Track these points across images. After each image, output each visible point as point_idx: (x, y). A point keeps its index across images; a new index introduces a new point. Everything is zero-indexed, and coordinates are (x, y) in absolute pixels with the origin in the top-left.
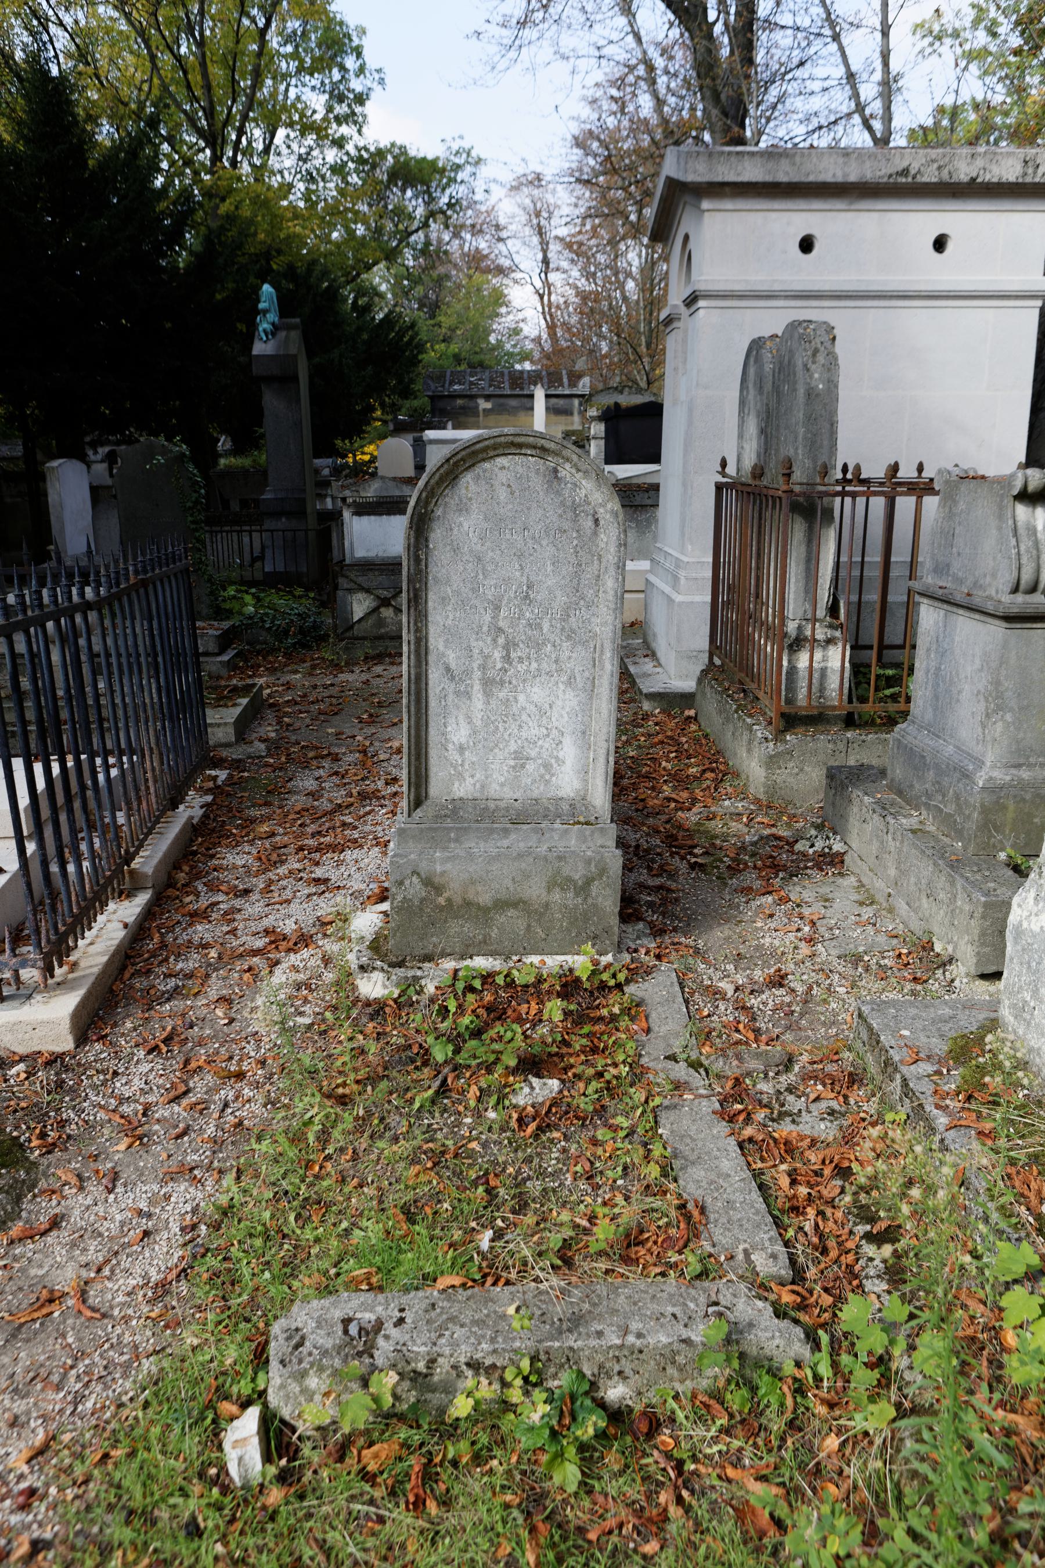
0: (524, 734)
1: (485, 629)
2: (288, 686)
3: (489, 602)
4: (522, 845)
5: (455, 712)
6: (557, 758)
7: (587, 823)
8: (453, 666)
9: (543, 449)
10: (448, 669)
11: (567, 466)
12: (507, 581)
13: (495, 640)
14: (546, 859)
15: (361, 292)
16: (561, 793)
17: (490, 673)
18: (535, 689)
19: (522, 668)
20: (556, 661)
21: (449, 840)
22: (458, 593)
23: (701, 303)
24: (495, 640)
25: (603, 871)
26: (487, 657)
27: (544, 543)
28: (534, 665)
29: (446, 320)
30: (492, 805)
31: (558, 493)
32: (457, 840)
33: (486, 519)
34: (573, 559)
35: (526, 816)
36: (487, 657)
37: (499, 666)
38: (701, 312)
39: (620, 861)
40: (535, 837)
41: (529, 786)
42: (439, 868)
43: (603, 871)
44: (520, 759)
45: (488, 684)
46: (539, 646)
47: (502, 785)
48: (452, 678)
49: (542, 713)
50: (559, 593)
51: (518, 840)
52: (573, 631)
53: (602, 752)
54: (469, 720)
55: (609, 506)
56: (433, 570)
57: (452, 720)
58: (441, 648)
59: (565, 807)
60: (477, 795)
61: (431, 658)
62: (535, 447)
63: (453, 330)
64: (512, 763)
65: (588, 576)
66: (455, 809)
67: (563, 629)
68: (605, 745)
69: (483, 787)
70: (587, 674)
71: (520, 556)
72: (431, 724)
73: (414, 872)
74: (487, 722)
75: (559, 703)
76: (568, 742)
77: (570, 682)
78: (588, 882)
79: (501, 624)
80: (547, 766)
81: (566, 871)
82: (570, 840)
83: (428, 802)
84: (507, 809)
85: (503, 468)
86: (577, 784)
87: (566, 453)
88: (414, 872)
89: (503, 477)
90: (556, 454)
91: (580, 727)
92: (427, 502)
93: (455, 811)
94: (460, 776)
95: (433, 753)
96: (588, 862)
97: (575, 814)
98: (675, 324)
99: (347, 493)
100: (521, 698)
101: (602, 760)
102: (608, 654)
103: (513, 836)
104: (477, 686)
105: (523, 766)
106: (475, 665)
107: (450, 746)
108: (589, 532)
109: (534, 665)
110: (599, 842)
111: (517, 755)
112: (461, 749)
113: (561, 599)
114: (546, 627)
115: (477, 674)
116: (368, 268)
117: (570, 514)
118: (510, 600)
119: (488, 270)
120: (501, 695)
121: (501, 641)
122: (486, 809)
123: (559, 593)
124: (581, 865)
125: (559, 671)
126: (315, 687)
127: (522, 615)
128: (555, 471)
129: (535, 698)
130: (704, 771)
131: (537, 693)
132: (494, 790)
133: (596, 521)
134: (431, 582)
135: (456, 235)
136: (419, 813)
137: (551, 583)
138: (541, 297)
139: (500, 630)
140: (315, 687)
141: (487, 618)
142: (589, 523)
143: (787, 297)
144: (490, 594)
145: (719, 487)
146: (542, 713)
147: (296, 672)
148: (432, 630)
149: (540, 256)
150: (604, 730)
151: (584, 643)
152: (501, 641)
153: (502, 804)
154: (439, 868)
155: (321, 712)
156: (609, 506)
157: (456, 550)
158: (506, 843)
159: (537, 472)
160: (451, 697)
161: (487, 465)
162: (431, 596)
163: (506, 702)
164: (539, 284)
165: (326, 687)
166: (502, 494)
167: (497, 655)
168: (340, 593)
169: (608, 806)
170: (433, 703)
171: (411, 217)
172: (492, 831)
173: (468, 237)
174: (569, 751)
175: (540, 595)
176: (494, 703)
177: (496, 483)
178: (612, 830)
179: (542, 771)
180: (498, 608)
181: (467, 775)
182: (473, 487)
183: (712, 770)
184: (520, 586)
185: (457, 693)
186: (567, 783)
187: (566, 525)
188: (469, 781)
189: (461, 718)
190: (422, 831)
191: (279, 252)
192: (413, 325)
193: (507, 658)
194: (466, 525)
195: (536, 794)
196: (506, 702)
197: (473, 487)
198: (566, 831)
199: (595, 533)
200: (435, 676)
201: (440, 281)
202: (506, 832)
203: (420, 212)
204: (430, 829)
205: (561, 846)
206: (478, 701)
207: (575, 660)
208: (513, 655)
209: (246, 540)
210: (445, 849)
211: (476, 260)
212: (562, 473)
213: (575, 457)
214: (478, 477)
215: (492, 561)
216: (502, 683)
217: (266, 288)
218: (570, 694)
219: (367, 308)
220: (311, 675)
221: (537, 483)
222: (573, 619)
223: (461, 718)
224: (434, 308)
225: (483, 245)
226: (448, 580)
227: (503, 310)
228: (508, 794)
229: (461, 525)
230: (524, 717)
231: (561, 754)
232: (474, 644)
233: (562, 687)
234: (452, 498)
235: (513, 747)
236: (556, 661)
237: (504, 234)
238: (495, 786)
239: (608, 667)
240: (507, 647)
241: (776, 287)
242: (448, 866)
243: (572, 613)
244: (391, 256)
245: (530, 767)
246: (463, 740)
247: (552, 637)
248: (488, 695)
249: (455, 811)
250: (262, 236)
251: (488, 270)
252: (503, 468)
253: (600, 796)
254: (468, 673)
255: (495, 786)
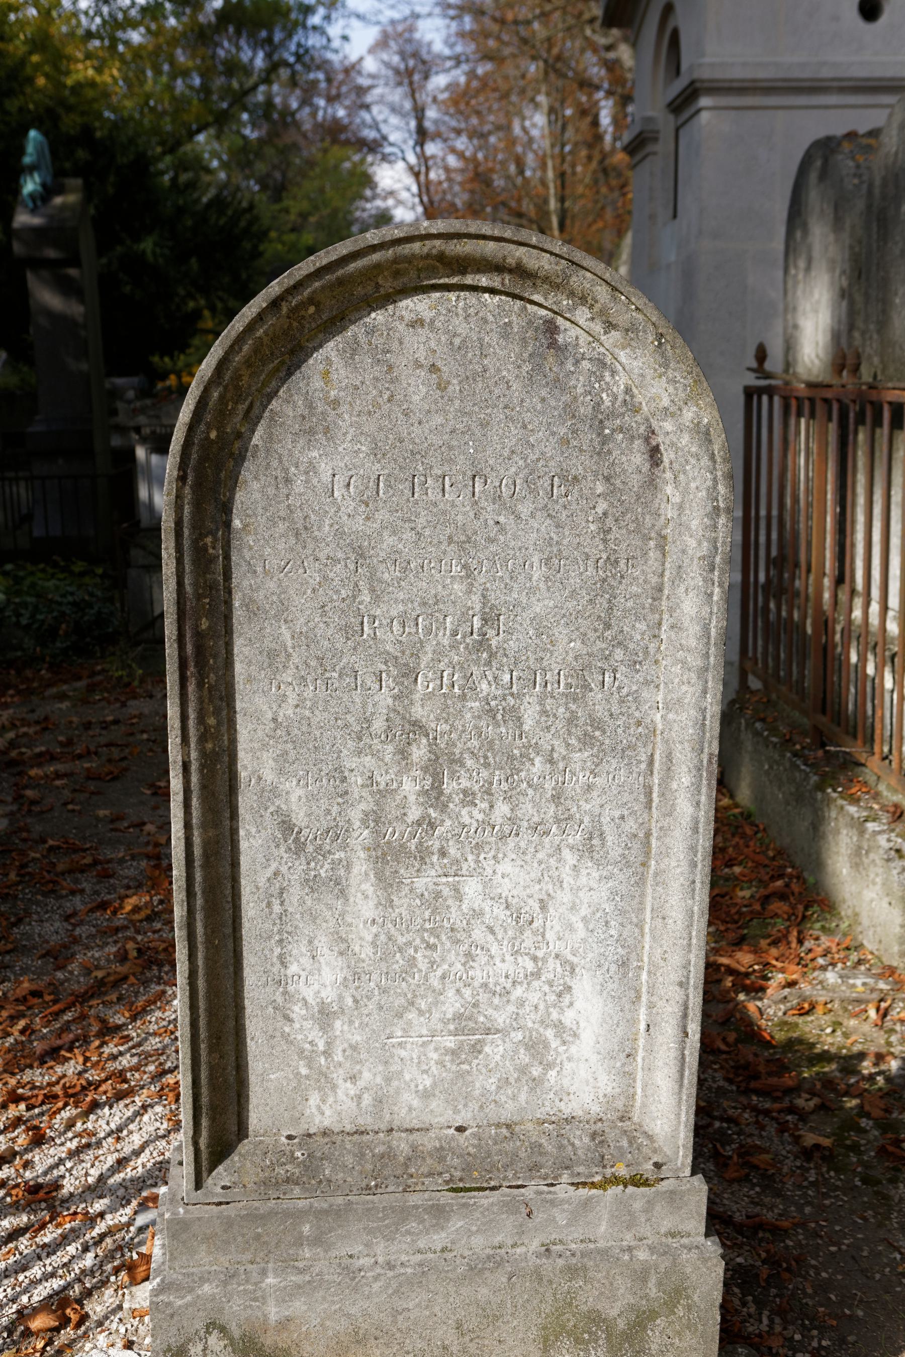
0: (478, 975)
1: (379, 725)
2: (45, 725)
3: (388, 659)
4: (478, 1241)
5: (307, 930)
6: (559, 1027)
7: (638, 1181)
8: (299, 818)
9: (520, 272)
10: (287, 826)
11: (582, 315)
12: (432, 606)
13: (403, 753)
14: (538, 1275)
15: (182, 166)
16: (569, 1108)
17: (395, 833)
18: (505, 867)
19: (471, 816)
20: (556, 798)
21: (299, 1242)
22: (307, 638)
23: (704, 101)
24: (403, 753)
25: (676, 1294)
26: (385, 793)
27: (524, 509)
28: (502, 809)
29: (295, 205)
30: (402, 1145)
31: (558, 384)
32: (317, 1241)
33: (376, 452)
34: (596, 549)
35: (484, 1169)
36: (385, 793)
37: (414, 814)
38: (705, 116)
39: (718, 1270)
40: (509, 1222)
41: (494, 1092)
42: (274, 1312)
43: (676, 1294)
44: (471, 1032)
45: (388, 859)
46: (513, 764)
47: (426, 1095)
48: (299, 848)
49: (522, 921)
50: (561, 633)
51: (470, 1231)
52: (597, 724)
53: (669, 1012)
54: (343, 945)
55: (689, 414)
56: (243, 583)
57: (298, 949)
58: (269, 776)
59: (581, 1141)
60: (366, 1121)
61: (246, 801)
62: (498, 268)
63: (304, 216)
64: (450, 1042)
65: (631, 591)
66: (312, 1160)
67: (572, 720)
68: (677, 995)
69: (379, 1101)
70: (630, 825)
71: (464, 543)
72: (250, 959)
73: (211, 1326)
74: (387, 949)
75: (564, 897)
76: (585, 987)
77: (591, 846)
78: (642, 1320)
79: (418, 712)
80: (536, 1047)
81: (589, 1298)
82: (602, 1222)
83: (244, 1147)
84: (440, 1153)
85: (417, 323)
86: (607, 1084)
87: (581, 281)
88: (211, 1326)
89: (417, 345)
90: (554, 284)
91: (615, 952)
92: (222, 414)
93: (311, 1165)
94: (324, 1081)
95: (254, 1028)
96: (642, 1275)
97: (603, 1158)
98: (650, 148)
99: (142, 420)
100: (471, 888)
101: (668, 1031)
102: (684, 779)
103: (457, 1223)
104: (361, 866)
105: (476, 1049)
106: (355, 815)
107: (297, 1010)
108: (635, 481)
109: (502, 809)
110: (666, 1225)
111: (462, 1023)
112: (325, 1015)
113: (567, 646)
114: (530, 715)
115: (362, 836)
116: (192, 134)
117: (588, 437)
118: (439, 654)
119: (347, 143)
120: (421, 883)
121: (419, 752)
122: (389, 1155)
123: (561, 633)
124: (622, 1285)
125: (564, 820)
126: (88, 726)
127: (470, 686)
128: (551, 329)
129: (505, 887)
130: (766, 900)
131: (511, 874)
132: (407, 1107)
133: (654, 453)
134: (239, 613)
135: (306, 101)
136: (222, 1175)
137: (542, 607)
138: (417, 175)
139: (417, 727)
140: (88, 726)
141: (384, 699)
142: (638, 458)
143: (842, 90)
144: (389, 639)
145: (750, 393)
146: (522, 921)
147: (62, 697)
148: (246, 733)
149: (413, 124)
150: (676, 959)
151: (625, 752)
152: (419, 752)
153: (428, 1142)
154: (274, 1312)
155: (91, 776)
156: (689, 414)
157: (301, 532)
158: (439, 1239)
159: (505, 332)
160: (295, 893)
161: (378, 317)
162: (240, 648)
163: (434, 901)
164: (412, 159)
165: (105, 725)
166: (417, 389)
167: (409, 787)
168: (133, 573)
169: (684, 1137)
170: (250, 909)
171: (247, 70)
172: (404, 1213)
173: (322, 103)
174: (589, 1008)
175: (514, 640)
176: (402, 904)
177: (401, 362)
178: (697, 1192)
179: (524, 1057)
180: (410, 674)
181: (338, 1076)
182: (341, 372)
183: (782, 896)
184: (465, 616)
185: (312, 884)
186: (582, 1082)
187: (579, 465)
188: (346, 1089)
189: (322, 942)
190: (229, 1223)
191: (69, 109)
192: (251, 207)
193: (435, 795)
194: (325, 469)
195: (509, 1110)
196: (434, 901)
197: (341, 372)
198: (586, 1204)
199: (652, 484)
200: (254, 843)
201: (286, 151)
202: (439, 1213)
203: (260, 61)
204: (253, 1217)
205: (573, 1238)
206: (364, 900)
207: (603, 793)
208: (449, 786)
209: (14, 489)
210: (288, 1264)
211: (335, 132)
212: (568, 334)
213: (602, 292)
214: (354, 348)
215: (394, 557)
216: (423, 854)
217: (33, 133)
218: (590, 874)
219: (192, 185)
220: (85, 702)
221: (506, 360)
222: (596, 696)
223: (322, 942)
224: (278, 191)
225: (341, 113)
226: (284, 607)
227: (368, 193)
228: (441, 1115)
229: (312, 468)
230: (479, 934)
231: (569, 1018)
232: (350, 762)
233: (570, 858)
234: (287, 406)
235: (452, 1004)
236: (556, 798)
237: (369, 99)
238: (409, 1098)
239: (685, 808)
240: (434, 769)
241: (826, 73)
242: (298, 1306)
243: (594, 680)
244: (221, 121)
245: (495, 1049)
246: (329, 995)
247: (546, 741)
248: (388, 883)
249: (311, 1165)
250: (41, 81)
251: (347, 143)
252: (417, 323)
253: (666, 1114)
254: (337, 833)
255: (409, 1098)
